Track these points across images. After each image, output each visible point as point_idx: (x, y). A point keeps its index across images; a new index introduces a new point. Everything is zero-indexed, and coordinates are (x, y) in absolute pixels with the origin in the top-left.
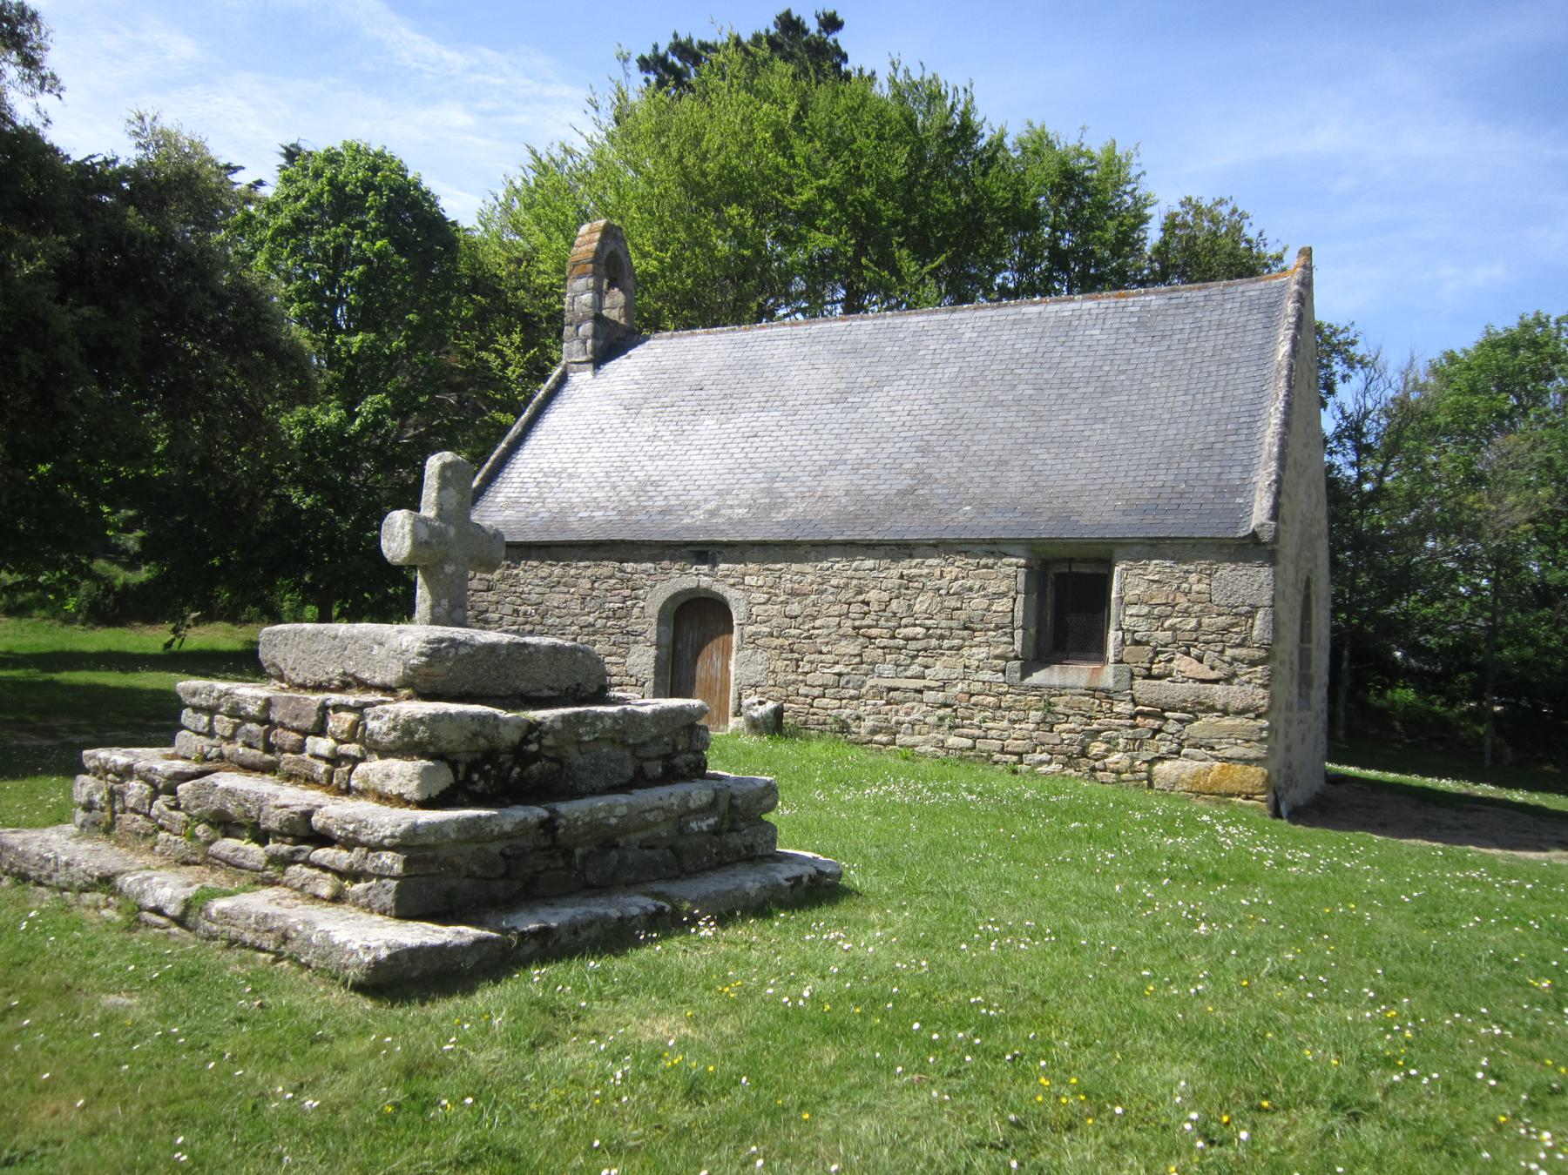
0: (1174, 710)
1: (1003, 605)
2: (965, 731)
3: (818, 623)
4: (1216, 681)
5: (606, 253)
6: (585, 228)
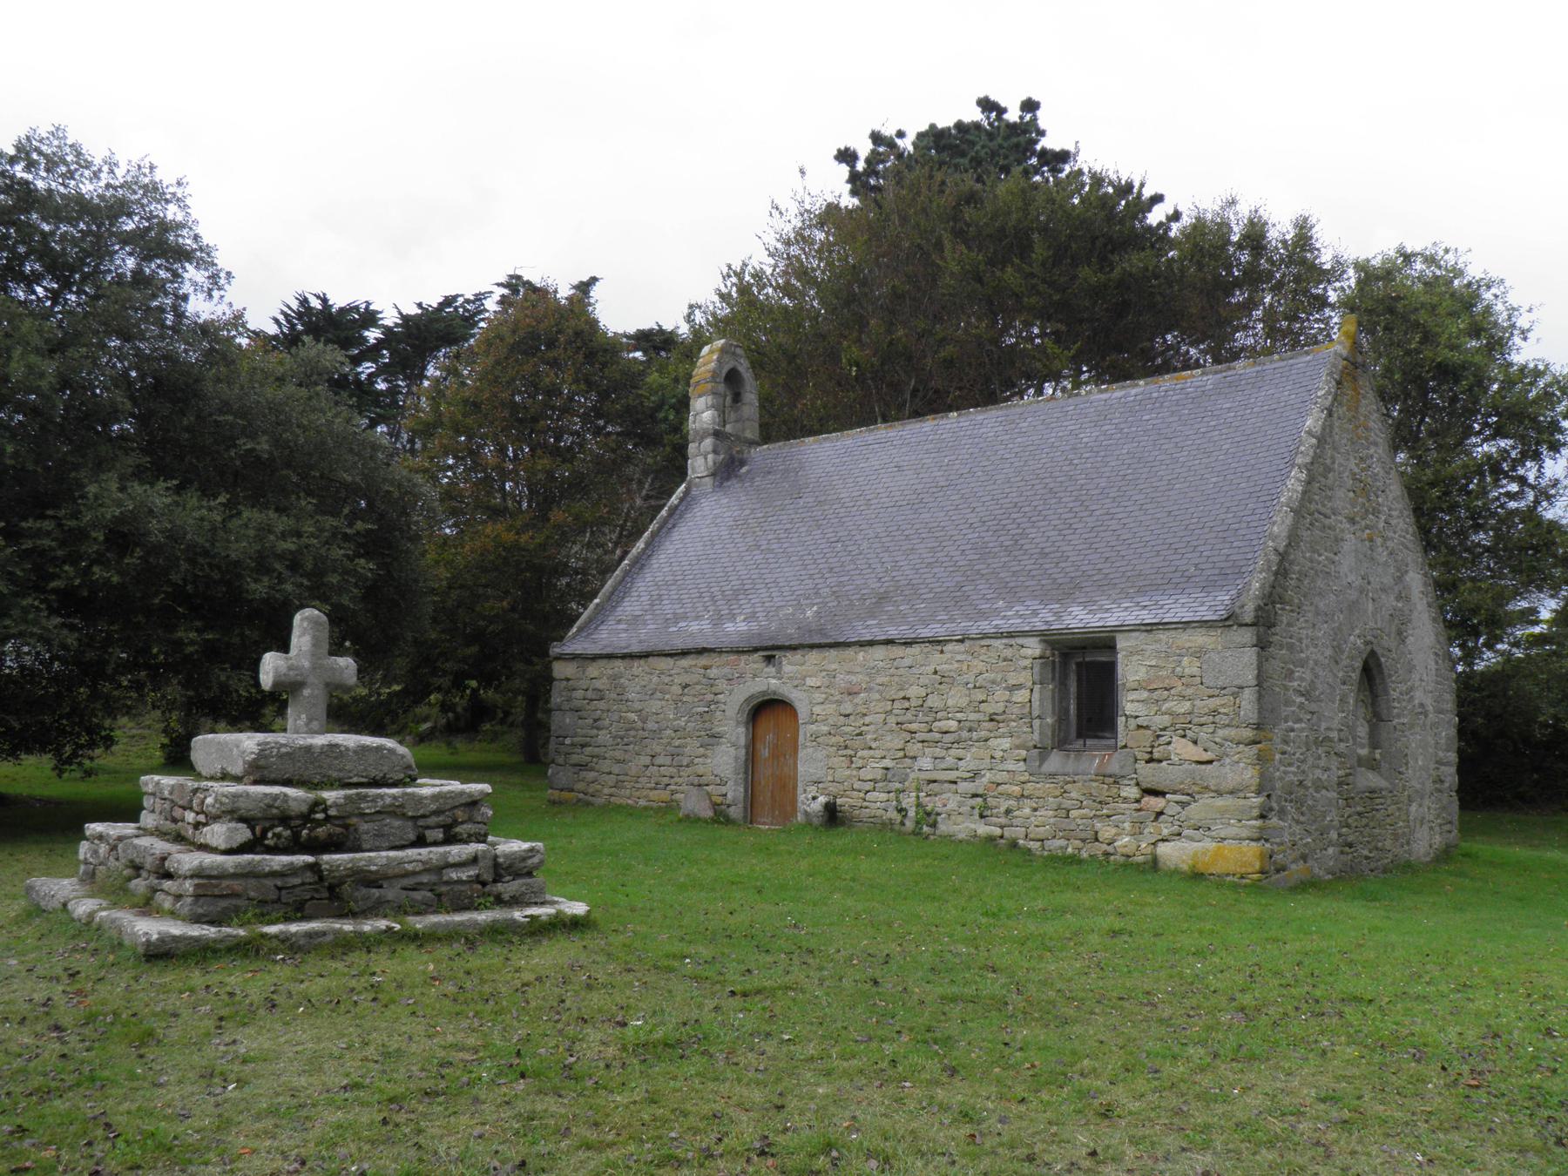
0: (1175, 793)
1: (1021, 696)
2: (994, 819)
3: (867, 720)
4: (1210, 762)
5: (724, 372)
6: (706, 349)
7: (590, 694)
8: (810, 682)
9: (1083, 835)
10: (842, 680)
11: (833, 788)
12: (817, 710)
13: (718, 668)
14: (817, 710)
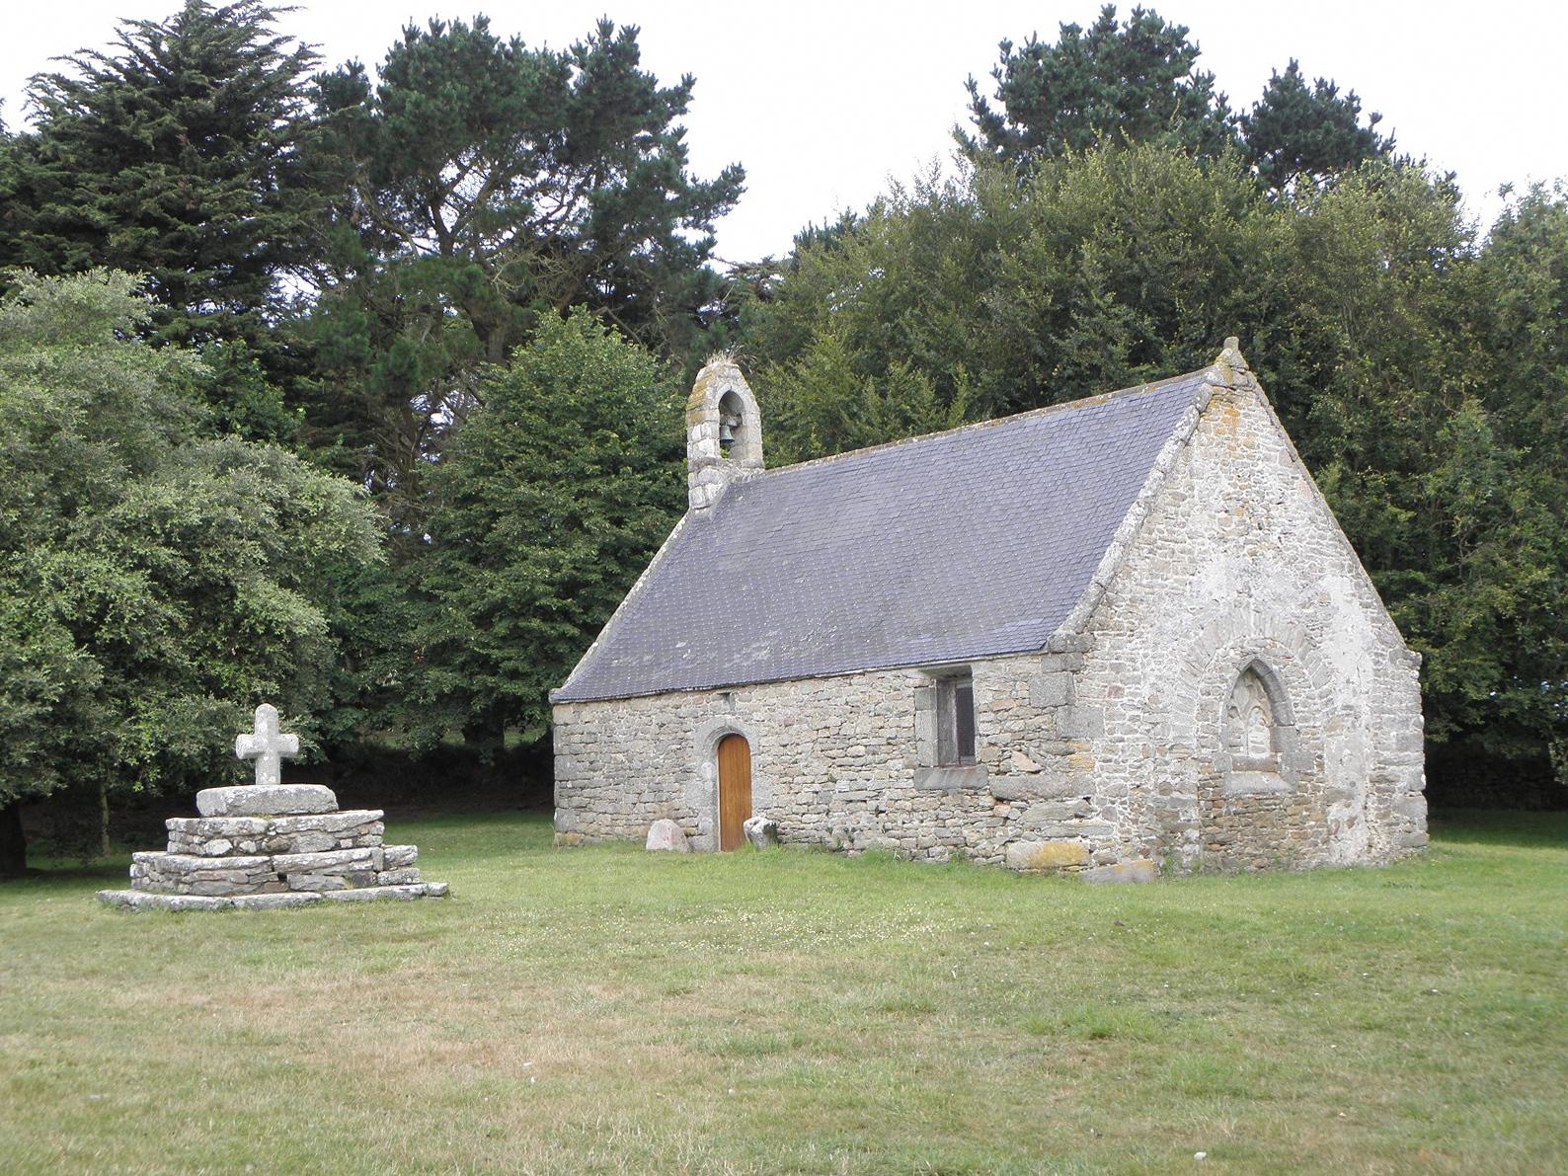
4: (1037, 772)
7: (585, 738)
8: (756, 716)
9: (955, 841)
10: (781, 714)
11: (777, 812)
12: (763, 741)
13: (688, 704)
14: (763, 741)
